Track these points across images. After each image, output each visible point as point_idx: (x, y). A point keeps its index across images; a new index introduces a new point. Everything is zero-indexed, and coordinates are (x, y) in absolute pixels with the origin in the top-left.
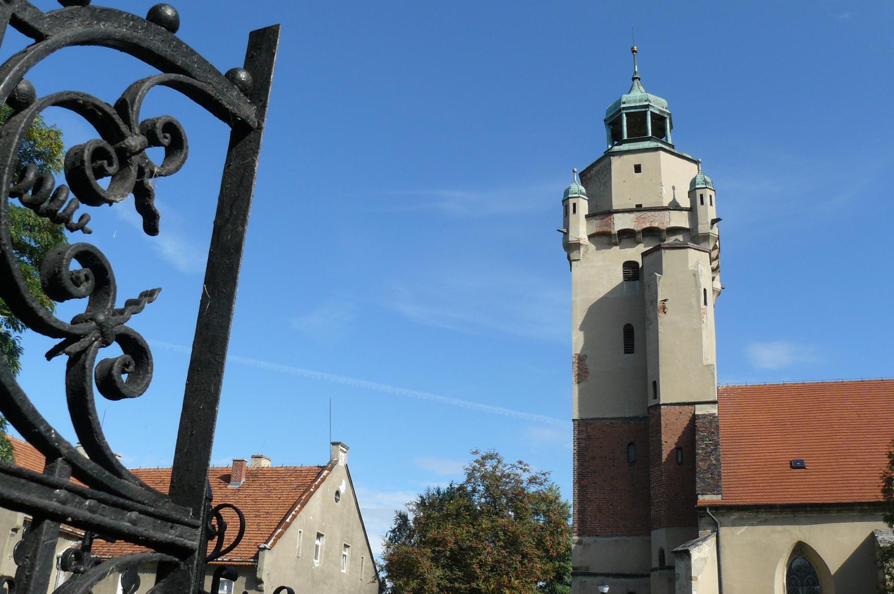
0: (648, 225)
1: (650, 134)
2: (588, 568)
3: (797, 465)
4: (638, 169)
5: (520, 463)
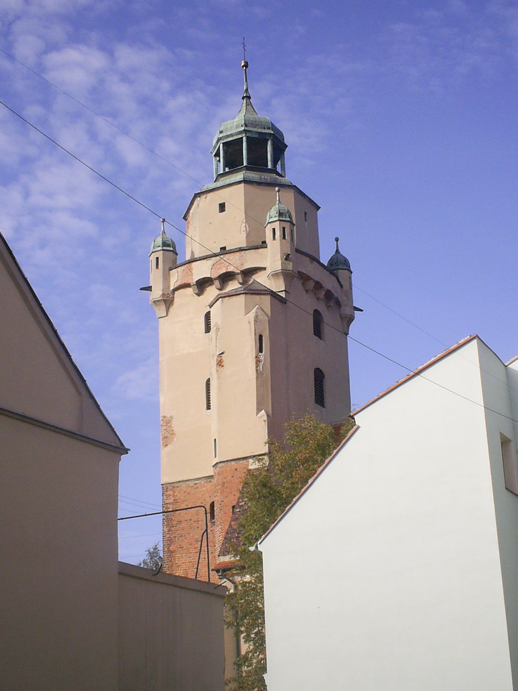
0: (224, 271)
4: (222, 207)
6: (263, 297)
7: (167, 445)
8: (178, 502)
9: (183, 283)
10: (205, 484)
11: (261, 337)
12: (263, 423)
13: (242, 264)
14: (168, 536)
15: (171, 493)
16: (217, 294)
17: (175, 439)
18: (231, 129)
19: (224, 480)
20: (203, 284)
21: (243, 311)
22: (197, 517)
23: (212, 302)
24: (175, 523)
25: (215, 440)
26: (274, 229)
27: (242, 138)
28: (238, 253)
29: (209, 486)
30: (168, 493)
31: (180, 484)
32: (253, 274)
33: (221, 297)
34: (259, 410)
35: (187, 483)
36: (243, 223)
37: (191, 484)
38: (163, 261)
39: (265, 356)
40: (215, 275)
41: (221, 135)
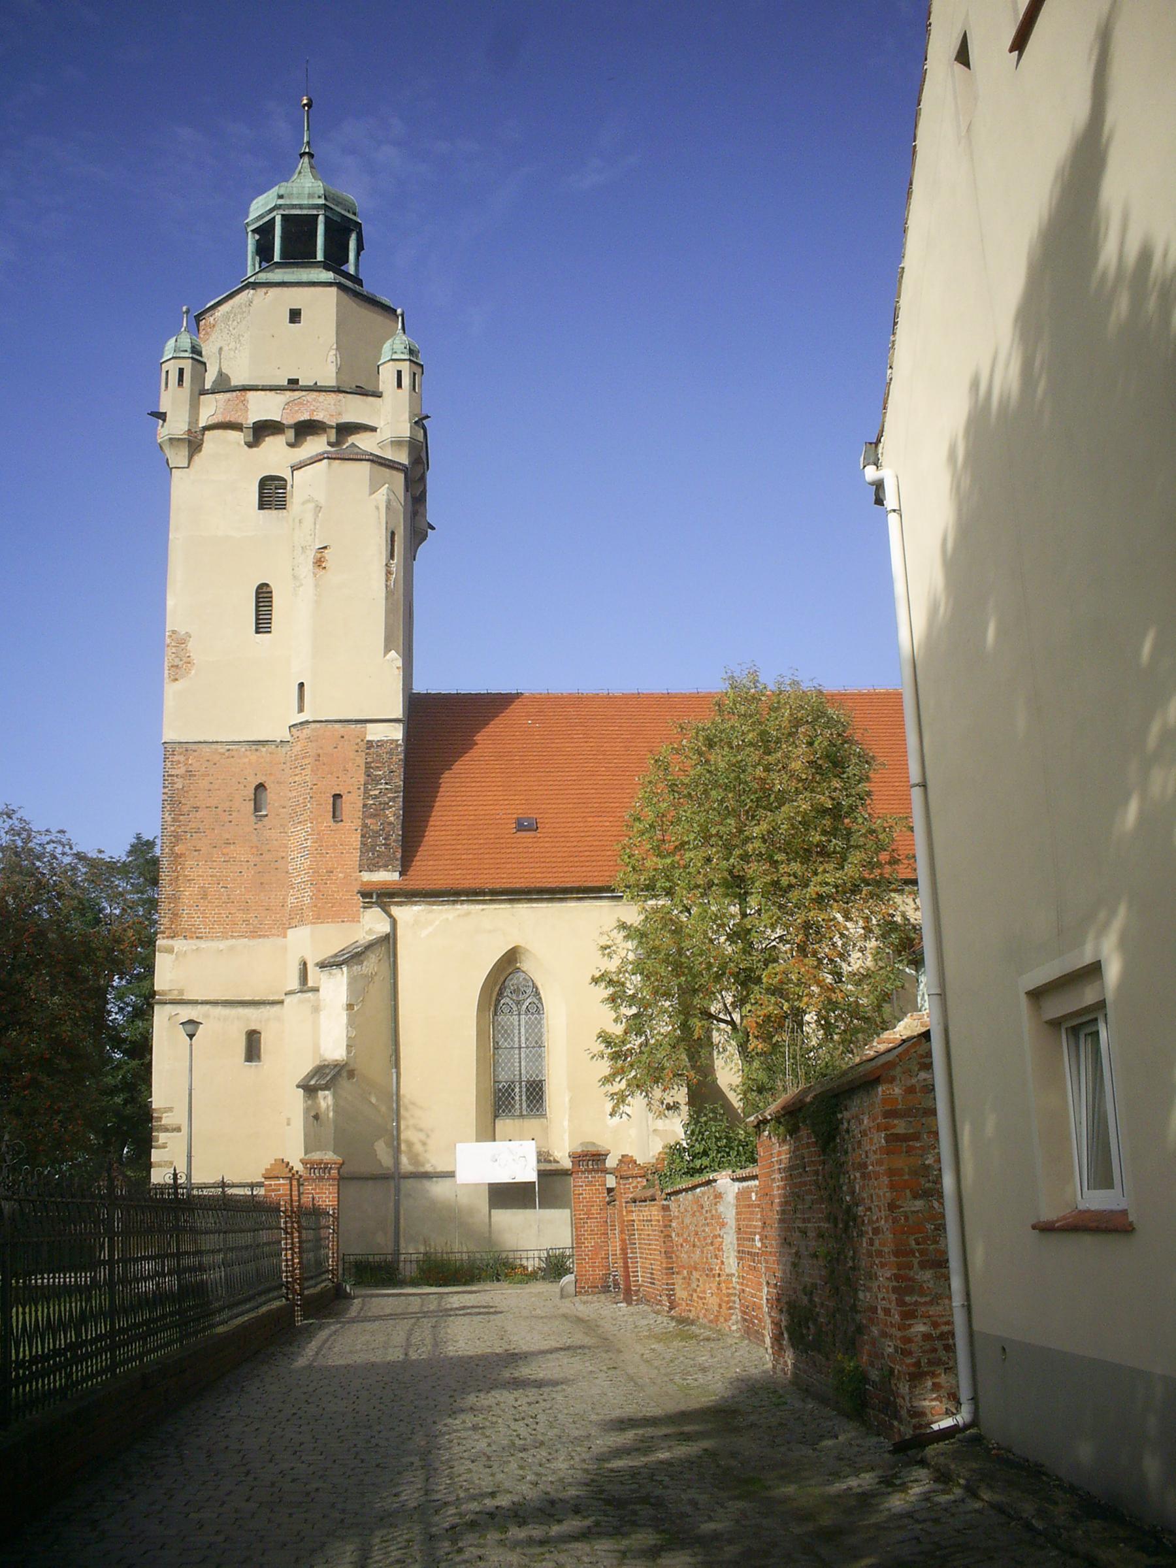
1: (320, 257)
2: (181, 992)
4: (295, 316)
9: (227, 419)
10: (248, 753)
11: (393, 534)
12: (396, 672)
13: (340, 414)
15: (182, 758)
16: (321, 450)
18: (299, 196)
19: (320, 751)
20: (263, 430)
21: (367, 490)
22: (228, 803)
24: (185, 809)
25: (301, 685)
26: (399, 373)
27: (274, 218)
29: (253, 757)
30: (176, 758)
31: (201, 746)
32: (352, 433)
34: (387, 650)
35: (214, 746)
36: (331, 349)
37: (222, 749)
40: (289, 420)
41: (280, 202)
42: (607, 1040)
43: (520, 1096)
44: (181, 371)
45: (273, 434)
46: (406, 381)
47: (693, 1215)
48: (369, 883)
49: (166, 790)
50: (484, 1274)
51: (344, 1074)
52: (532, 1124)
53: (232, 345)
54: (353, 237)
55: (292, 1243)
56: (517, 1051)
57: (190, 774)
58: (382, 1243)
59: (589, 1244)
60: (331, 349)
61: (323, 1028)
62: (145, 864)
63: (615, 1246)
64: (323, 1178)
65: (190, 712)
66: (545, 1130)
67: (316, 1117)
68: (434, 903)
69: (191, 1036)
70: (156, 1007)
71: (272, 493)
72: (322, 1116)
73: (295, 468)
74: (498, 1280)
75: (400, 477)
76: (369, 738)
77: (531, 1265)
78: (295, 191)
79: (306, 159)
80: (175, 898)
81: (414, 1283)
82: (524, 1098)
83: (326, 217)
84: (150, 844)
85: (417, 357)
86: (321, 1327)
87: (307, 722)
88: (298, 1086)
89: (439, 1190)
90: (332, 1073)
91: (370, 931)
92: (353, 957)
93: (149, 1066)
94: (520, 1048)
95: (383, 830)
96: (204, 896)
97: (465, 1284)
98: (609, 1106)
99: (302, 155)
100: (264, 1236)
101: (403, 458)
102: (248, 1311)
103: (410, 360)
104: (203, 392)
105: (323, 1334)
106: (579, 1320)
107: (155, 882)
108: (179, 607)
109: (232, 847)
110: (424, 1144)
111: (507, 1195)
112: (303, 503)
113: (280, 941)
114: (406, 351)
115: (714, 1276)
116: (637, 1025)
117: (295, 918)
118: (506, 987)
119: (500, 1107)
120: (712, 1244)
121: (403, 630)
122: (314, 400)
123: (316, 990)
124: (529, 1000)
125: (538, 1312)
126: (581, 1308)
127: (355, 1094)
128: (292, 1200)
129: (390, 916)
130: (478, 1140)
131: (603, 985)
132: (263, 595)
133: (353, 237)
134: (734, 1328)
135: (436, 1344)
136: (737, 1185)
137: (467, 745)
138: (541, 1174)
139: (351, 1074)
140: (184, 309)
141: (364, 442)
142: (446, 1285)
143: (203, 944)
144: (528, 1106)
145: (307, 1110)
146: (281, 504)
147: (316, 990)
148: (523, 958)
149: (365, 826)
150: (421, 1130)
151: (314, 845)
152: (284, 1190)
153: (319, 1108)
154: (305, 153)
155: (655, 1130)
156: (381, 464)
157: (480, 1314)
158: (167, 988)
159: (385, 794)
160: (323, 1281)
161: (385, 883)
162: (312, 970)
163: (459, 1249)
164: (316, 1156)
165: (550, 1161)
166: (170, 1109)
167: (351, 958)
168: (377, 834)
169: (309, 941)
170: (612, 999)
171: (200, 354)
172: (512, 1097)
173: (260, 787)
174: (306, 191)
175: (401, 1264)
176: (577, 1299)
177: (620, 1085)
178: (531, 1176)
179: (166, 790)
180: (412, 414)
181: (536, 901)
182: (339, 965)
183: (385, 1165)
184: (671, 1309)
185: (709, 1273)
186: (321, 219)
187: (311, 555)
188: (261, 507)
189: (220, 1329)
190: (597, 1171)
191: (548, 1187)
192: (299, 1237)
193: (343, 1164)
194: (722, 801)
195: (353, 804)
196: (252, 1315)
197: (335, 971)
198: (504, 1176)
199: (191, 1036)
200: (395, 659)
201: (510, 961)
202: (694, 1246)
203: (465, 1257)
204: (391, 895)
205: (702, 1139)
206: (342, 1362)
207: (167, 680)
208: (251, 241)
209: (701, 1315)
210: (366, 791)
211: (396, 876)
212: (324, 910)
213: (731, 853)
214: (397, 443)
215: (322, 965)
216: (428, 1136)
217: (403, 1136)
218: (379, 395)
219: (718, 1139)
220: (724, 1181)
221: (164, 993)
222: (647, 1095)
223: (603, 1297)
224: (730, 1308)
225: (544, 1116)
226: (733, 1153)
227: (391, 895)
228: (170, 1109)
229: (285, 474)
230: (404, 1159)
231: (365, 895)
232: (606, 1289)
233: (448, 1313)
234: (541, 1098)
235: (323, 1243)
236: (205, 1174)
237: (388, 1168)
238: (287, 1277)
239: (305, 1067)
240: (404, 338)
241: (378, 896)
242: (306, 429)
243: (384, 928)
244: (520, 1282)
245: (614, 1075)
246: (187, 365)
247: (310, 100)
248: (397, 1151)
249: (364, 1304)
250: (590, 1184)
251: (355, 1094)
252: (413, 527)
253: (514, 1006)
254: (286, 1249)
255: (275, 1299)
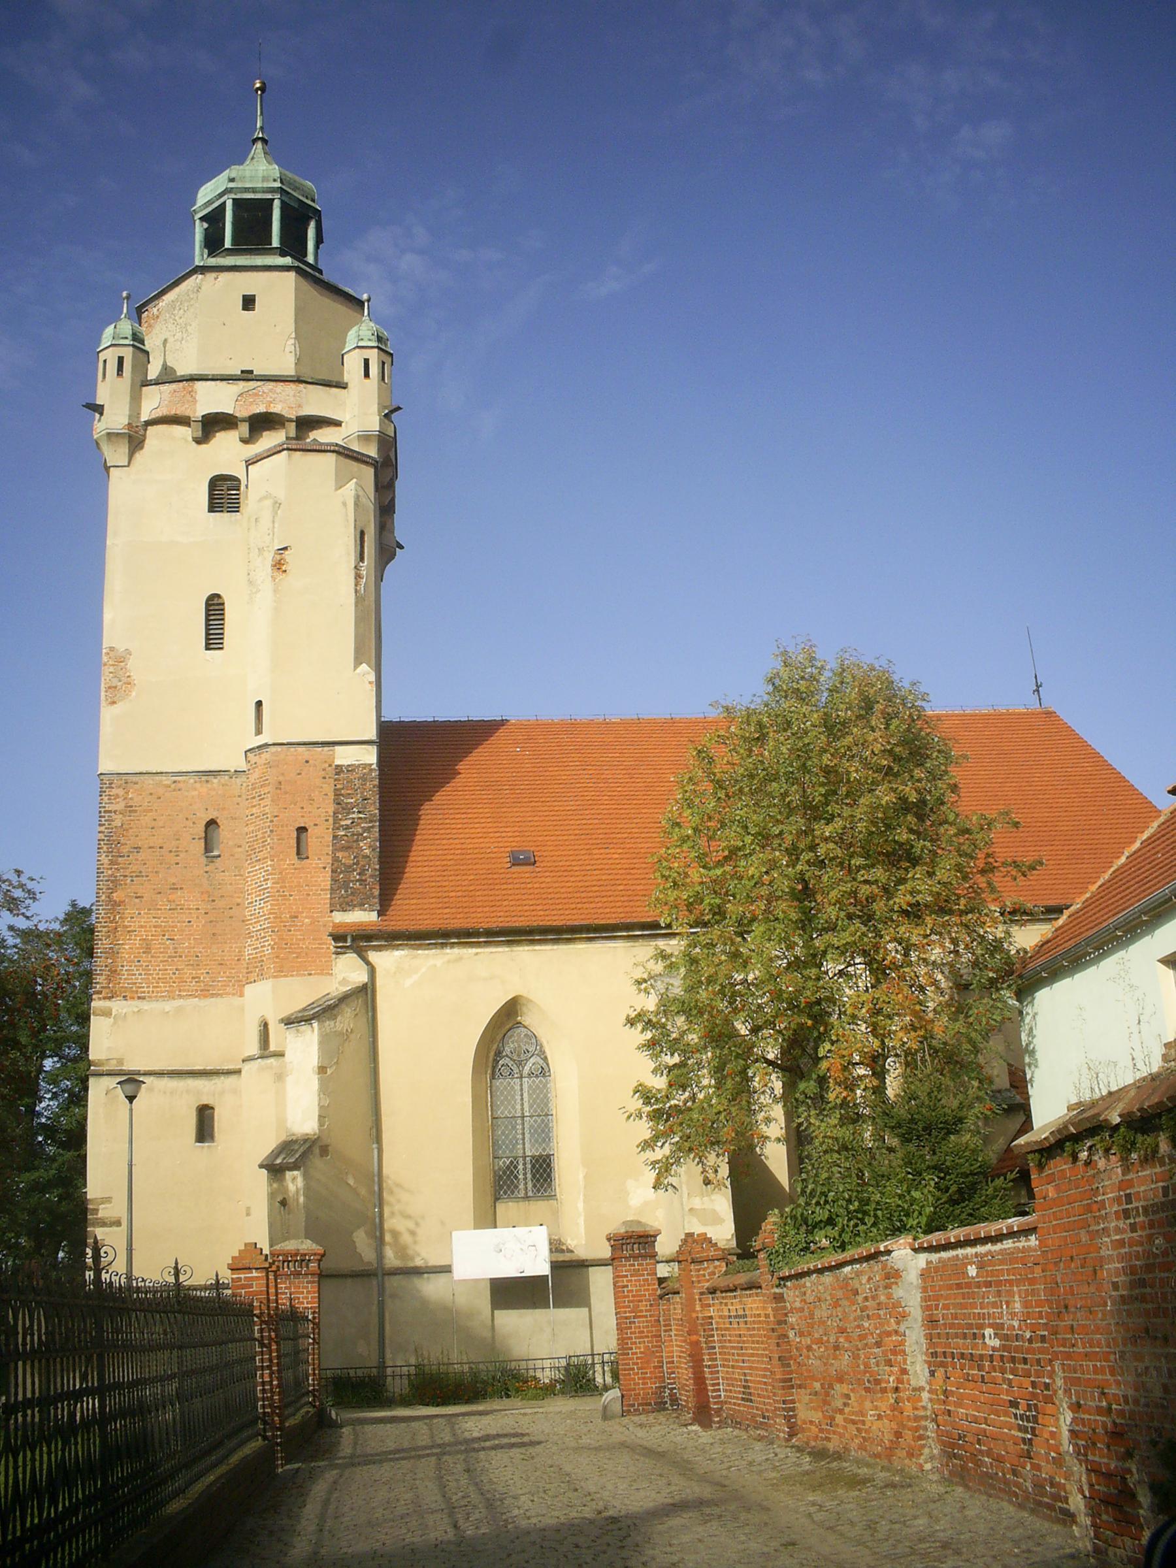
0: (261, 409)
1: (276, 243)
2: (120, 1061)
3: (521, 860)
4: (249, 302)
5: (19, 873)
6: (363, 466)
7: (114, 703)
8: (135, 811)
9: (173, 412)
10: (198, 785)
11: (362, 533)
12: (369, 687)
14: (110, 872)
15: (120, 792)
17: (134, 694)
18: (252, 178)
19: (281, 778)
20: (213, 424)
22: (174, 843)
23: (256, 455)
24: (125, 850)
25: (259, 704)
26: (366, 362)
28: (292, 385)
29: (204, 789)
30: (114, 792)
31: (142, 777)
32: (313, 428)
33: (288, 449)
35: (157, 778)
36: (289, 337)
37: (167, 780)
38: (134, 367)
39: (368, 568)
40: (243, 411)
41: (231, 185)
42: (646, 1095)
43: (523, 1172)
44: (121, 360)
45: (224, 429)
46: (374, 370)
47: (836, 1305)
48: (340, 925)
49: (102, 829)
50: (489, 1390)
51: (317, 1151)
52: (539, 1207)
53: (179, 335)
54: (312, 224)
55: (270, 1360)
56: (519, 1121)
57: (130, 809)
58: (363, 1355)
59: (638, 1349)
60: (289, 337)
61: (291, 1097)
62: (80, 924)
63: (676, 1348)
64: (299, 1274)
65: (127, 741)
66: (556, 1213)
67: (283, 1203)
68: (419, 947)
69: (131, 1098)
70: (92, 1081)
71: (223, 494)
72: (290, 1202)
73: (249, 463)
74: (508, 1396)
75: (370, 472)
76: (338, 762)
77: (545, 1377)
78: (248, 174)
79: (259, 145)
80: (113, 953)
81: (406, 1402)
82: (529, 1176)
83: (283, 202)
84: (86, 912)
85: (386, 345)
86: (312, 1476)
87: (266, 745)
88: (261, 1166)
89: (432, 1288)
90: (302, 1150)
91: (344, 981)
92: (325, 1010)
93: (84, 1158)
94: (523, 1117)
95: (357, 864)
96: (148, 950)
97: (468, 1401)
98: (652, 1175)
99: (255, 141)
100: (234, 1351)
101: (372, 451)
102: (215, 1465)
103: (378, 347)
104: (146, 383)
105: (319, 1489)
106: (649, 1452)
107: (90, 953)
108: (120, 620)
109: (179, 893)
110: (413, 1233)
111: (513, 1292)
112: (261, 500)
113: (236, 1001)
114: (374, 338)
115: (884, 1390)
116: (680, 1078)
117: (255, 971)
118: (504, 1042)
119: (501, 1187)
120: (878, 1344)
121: (372, 643)
122: (271, 390)
123: (281, 1055)
124: (532, 1060)
125: (585, 1441)
126: (641, 1433)
127: (328, 1174)
128: (268, 1300)
129: (368, 963)
130: (476, 1228)
131: (640, 1026)
132: (214, 607)
133: (312, 224)
134: (928, 1466)
135: (490, 1505)
136: (922, 1259)
137: (447, 774)
138: (556, 1266)
139: (324, 1151)
140: (125, 294)
141: (323, 436)
142: (444, 1402)
143: (145, 1005)
144: (534, 1186)
145: (272, 1196)
146: (233, 506)
147: (281, 1055)
148: (524, 1009)
149: (335, 859)
150: (409, 1217)
151: (280, 886)
152: (258, 1286)
153: (286, 1190)
154: (258, 139)
155: (691, 1210)
156: (347, 456)
157: (513, 1445)
158: (103, 1057)
159: (359, 824)
160: (302, 1406)
161: (361, 924)
162: (275, 1029)
163: (457, 1359)
164: (290, 1245)
165: (562, 1251)
166: (108, 1200)
167: (324, 1012)
168: (349, 869)
169: (267, 998)
170: (651, 1044)
171: (142, 342)
172: (516, 1175)
173: (212, 823)
174: (260, 174)
175: (389, 1379)
176: (625, 1420)
177: (661, 1152)
178: (544, 1269)
179: (102, 829)
180: (381, 406)
181: (540, 942)
182: (308, 1020)
183: (366, 1260)
184: (791, 1435)
185: (875, 1386)
186: (277, 203)
187: (269, 557)
188: (212, 508)
189: (174, 1507)
190: (644, 1257)
191: (564, 1281)
192: (278, 1350)
193: (323, 1255)
194: (785, 795)
195: (320, 839)
196: (222, 1469)
197: (305, 1028)
198: (509, 1270)
199: (131, 1098)
200: (366, 671)
201: (509, 1015)
202: (837, 1348)
203: (466, 1368)
204: (369, 937)
205: (826, 1202)
206: (361, 1547)
207: (103, 703)
208: (199, 229)
209: (854, 1445)
210: (336, 820)
211: (373, 916)
212: (288, 961)
213: (798, 859)
214: (365, 438)
215: (289, 1022)
216: (417, 1224)
217: (386, 1226)
218: (343, 386)
219: (849, 1201)
220: (903, 1252)
221: (99, 1063)
222: (700, 1161)
223: (661, 1417)
224: (921, 1438)
225: (553, 1197)
226: (869, 1221)
227: (369, 937)
228: (108, 1200)
229: (239, 472)
230: (389, 1253)
231: (338, 937)
232: (660, 1406)
233: (471, 1446)
234: (549, 1176)
235: (303, 1356)
236: (151, 1270)
237: (369, 1263)
238: (264, 1406)
239: (267, 1145)
240: (372, 324)
241: (354, 939)
242: (262, 423)
243: (362, 977)
244: (535, 1398)
245: (656, 1138)
246: (128, 354)
247: (263, 84)
248: (380, 1242)
249: (356, 1435)
250: (636, 1273)
251: (328, 1174)
252: (382, 542)
253: (515, 1068)
254: (262, 1368)
255: (250, 1438)
